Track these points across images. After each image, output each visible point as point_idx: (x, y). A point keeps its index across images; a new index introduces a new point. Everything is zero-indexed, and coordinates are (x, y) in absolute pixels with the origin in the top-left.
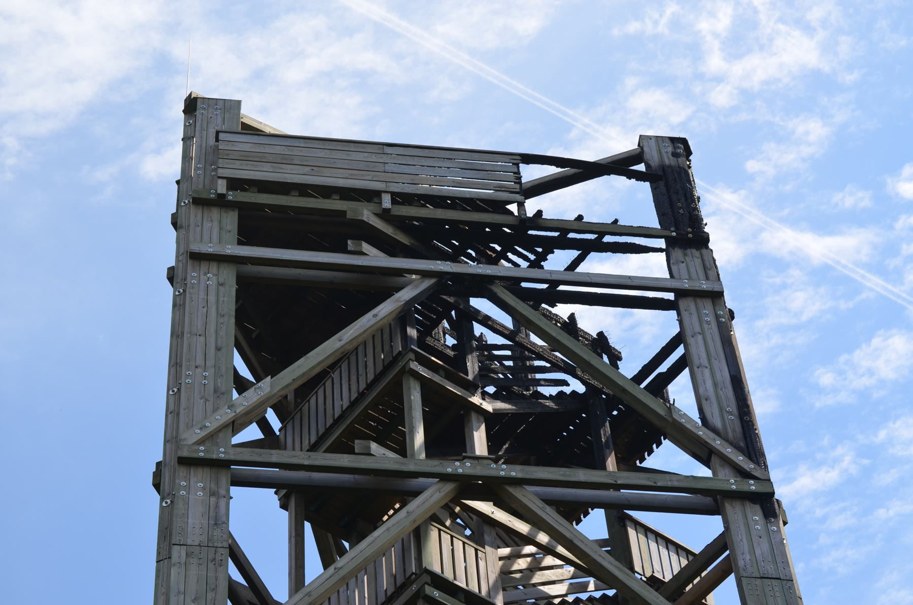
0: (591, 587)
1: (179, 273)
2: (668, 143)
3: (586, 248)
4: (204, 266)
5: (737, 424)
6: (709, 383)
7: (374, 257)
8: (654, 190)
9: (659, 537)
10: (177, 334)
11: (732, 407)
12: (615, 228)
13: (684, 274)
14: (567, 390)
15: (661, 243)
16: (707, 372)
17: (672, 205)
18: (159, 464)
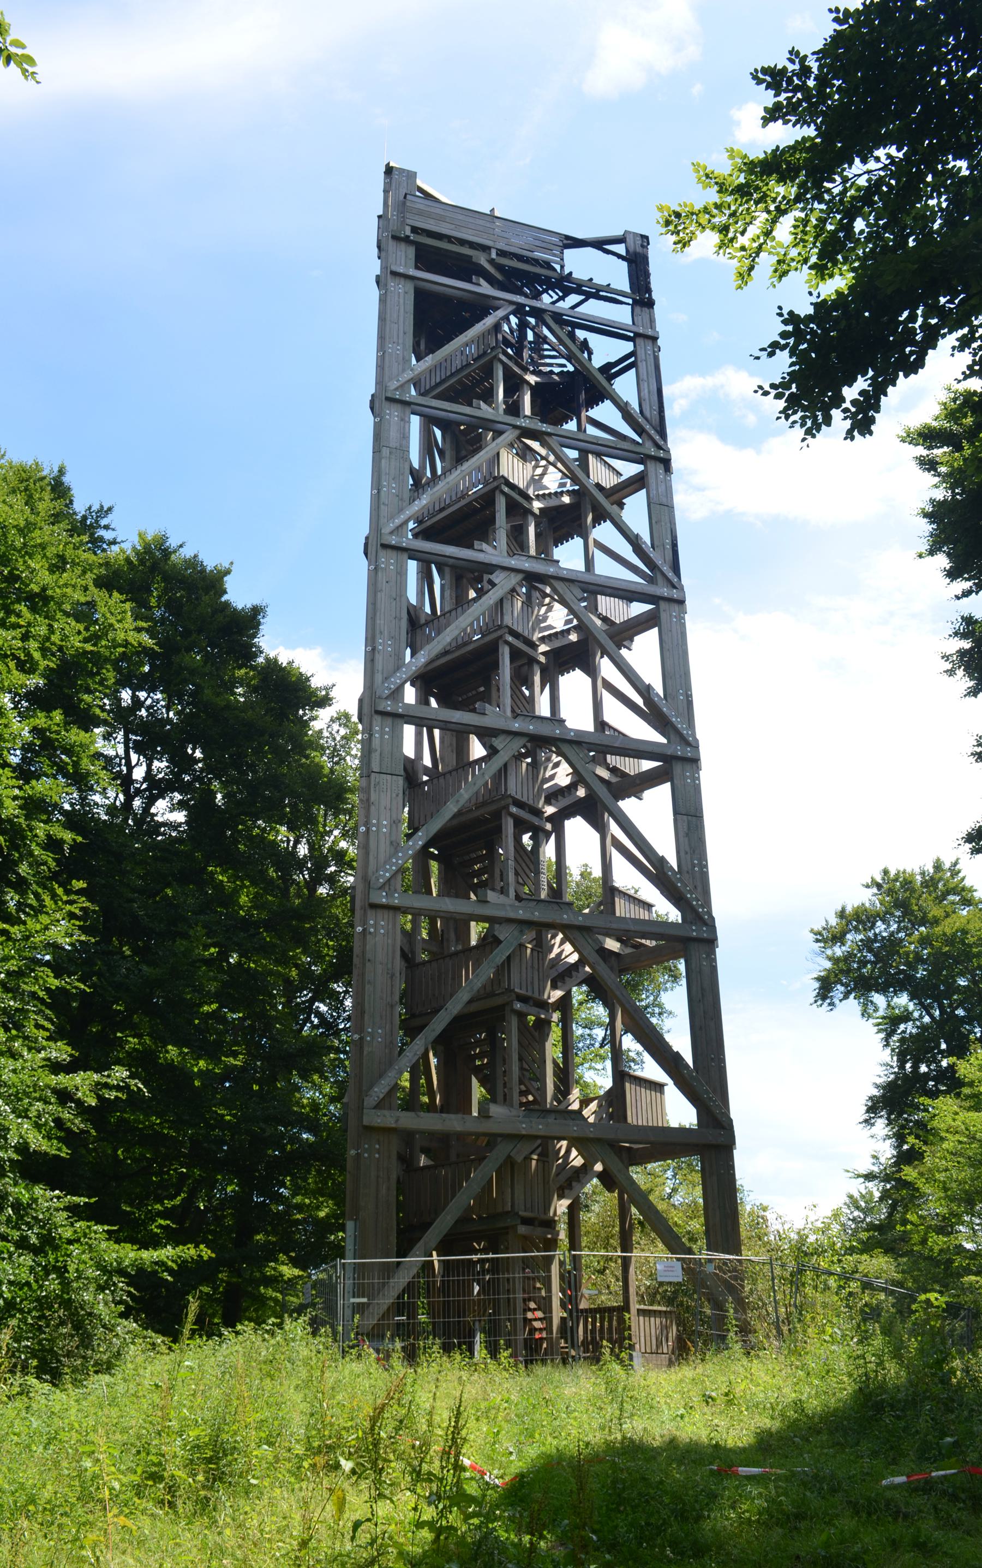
0: (568, 485)
1: (382, 280)
2: (639, 238)
3: (588, 296)
4: (397, 279)
5: (658, 416)
6: (646, 391)
7: (485, 288)
8: (629, 267)
9: (610, 466)
10: (382, 319)
11: (656, 407)
12: (608, 288)
13: (640, 324)
14: (565, 370)
15: (630, 301)
16: (646, 384)
17: (638, 278)
18: (373, 396)
